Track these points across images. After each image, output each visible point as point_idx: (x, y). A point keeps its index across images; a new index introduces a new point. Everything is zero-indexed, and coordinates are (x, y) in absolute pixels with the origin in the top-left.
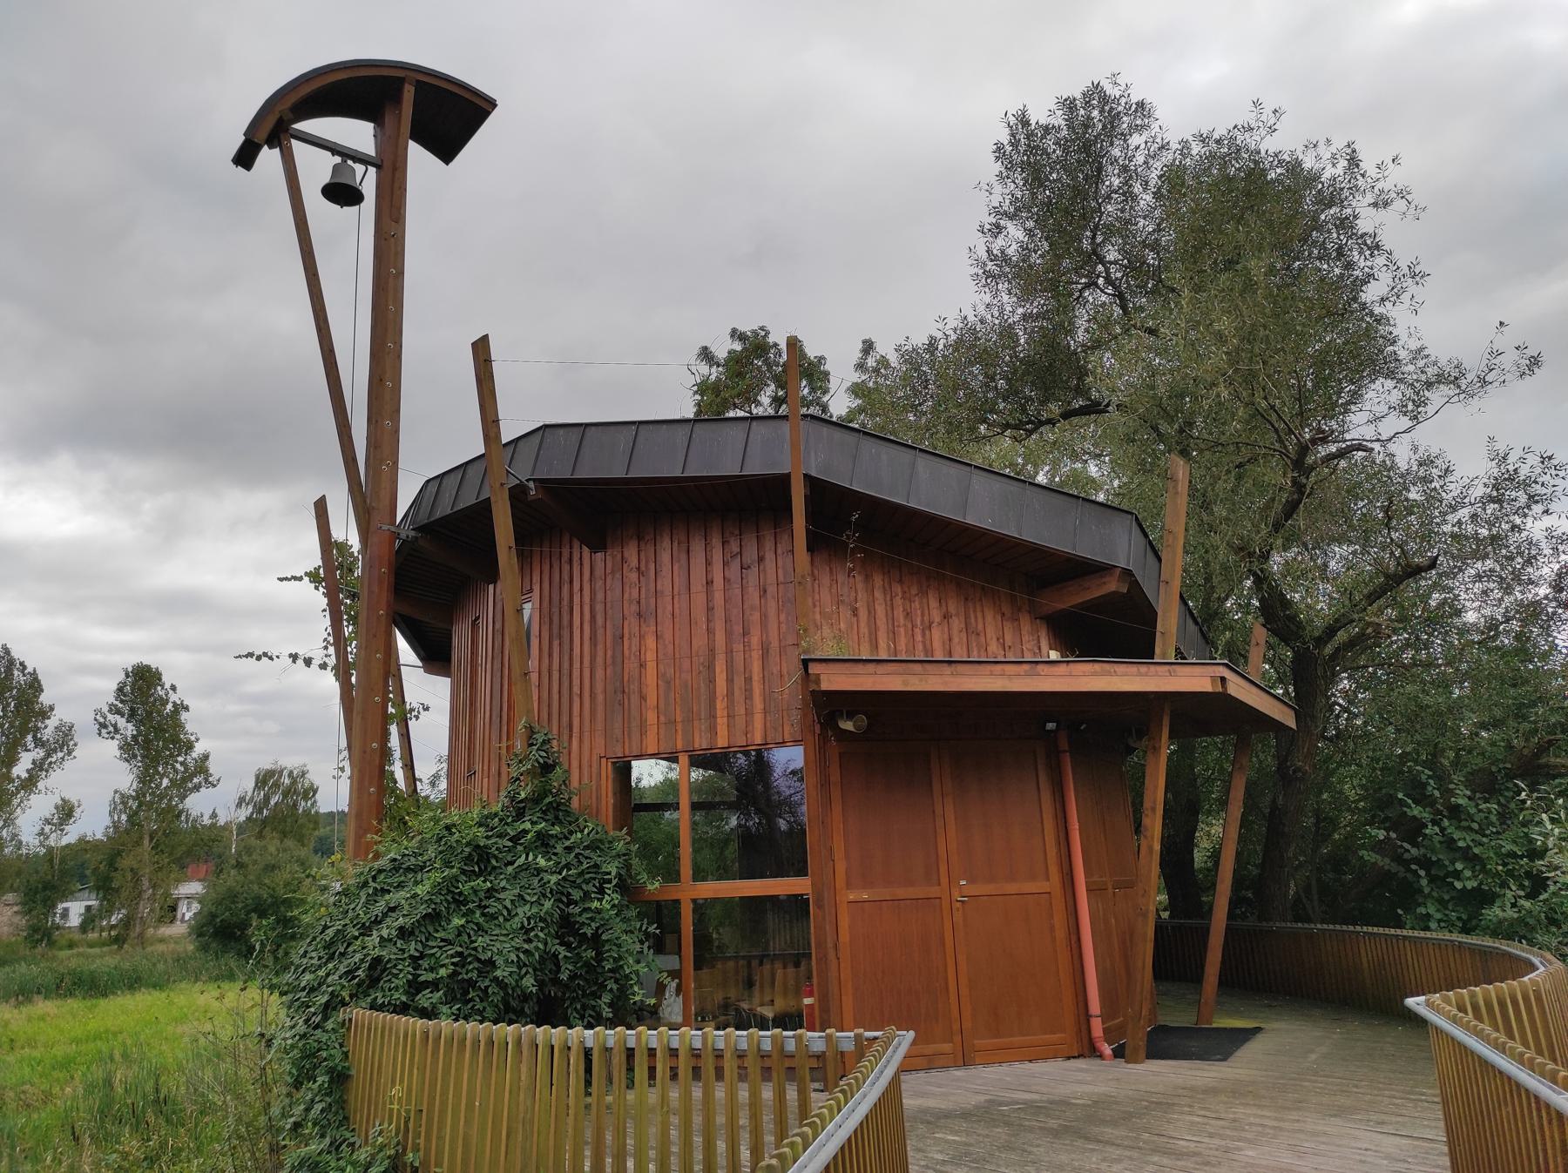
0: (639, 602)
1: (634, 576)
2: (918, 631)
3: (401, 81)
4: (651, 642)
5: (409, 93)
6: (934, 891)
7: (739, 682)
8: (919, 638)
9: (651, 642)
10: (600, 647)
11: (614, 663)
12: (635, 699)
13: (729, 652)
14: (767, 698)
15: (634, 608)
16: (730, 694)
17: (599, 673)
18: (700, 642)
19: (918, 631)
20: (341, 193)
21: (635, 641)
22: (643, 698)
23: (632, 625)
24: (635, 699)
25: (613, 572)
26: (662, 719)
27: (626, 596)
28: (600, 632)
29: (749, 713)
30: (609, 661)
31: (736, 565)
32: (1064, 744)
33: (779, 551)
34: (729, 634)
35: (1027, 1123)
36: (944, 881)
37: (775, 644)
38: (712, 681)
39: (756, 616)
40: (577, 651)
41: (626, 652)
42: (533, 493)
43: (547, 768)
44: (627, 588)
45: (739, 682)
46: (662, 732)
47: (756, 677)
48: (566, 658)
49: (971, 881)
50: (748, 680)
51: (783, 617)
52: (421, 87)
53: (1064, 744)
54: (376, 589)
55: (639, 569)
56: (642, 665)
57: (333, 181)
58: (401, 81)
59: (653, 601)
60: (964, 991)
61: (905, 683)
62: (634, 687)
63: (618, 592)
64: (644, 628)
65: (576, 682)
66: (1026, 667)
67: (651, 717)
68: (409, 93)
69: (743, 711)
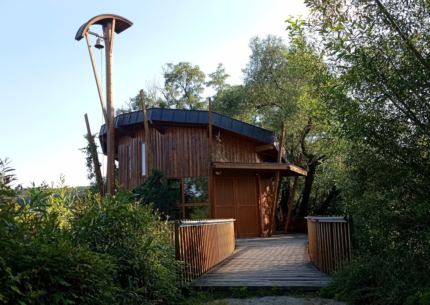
0: (172, 146)
1: (171, 140)
2: (231, 155)
3: (112, 19)
4: (175, 154)
5: (114, 22)
6: (233, 206)
7: (195, 164)
8: (231, 156)
9: (175, 154)
10: (164, 155)
11: (167, 158)
12: (172, 166)
13: (192, 157)
14: (201, 167)
15: (171, 147)
16: (193, 166)
17: (164, 161)
18: (186, 155)
19: (231, 155)
20: (98, 46)
21: (172, 154)
22: (174, 166)
23: (171, 151)
24: (172, 166)
25: (166, 139)
26: (178, 171)
27: (169, 144)
28: (164, 152)
29: (197, 171)
30: (166, 158)
31: (194, 139)
32: (259, 178)
33: (203, 137)
34: (192, 154)
35: (199, 173)
36: (235, 203)
37: (202, 157)
38: (189, 163)
39: (198, 150)
40: (158, 155)
41: (170, 156)
42: (151, 123)
43: (219, 67)
44: (170, 143)
45: (195, 164)
46: (178, 173)
47: (198, 163)
48: (155, 157)
49: (240, 204)
50: (197, 164)
51: (204, 151)
52: (116, 20)
53: (259, 178)
54: (111, 140)
55: (172, 139)
56: (173, 159)
57: (97, 44)
58: (112, 19)
59: (175, 146)
60: (238, 224)
61: (231, 167)
62: (172, 164)
63: (168, 143)
64: (173, 151)
65: (158, 162)
66: (253, 164)
67: (176, 170)
68: (114, 22)
69: (195, 170)
